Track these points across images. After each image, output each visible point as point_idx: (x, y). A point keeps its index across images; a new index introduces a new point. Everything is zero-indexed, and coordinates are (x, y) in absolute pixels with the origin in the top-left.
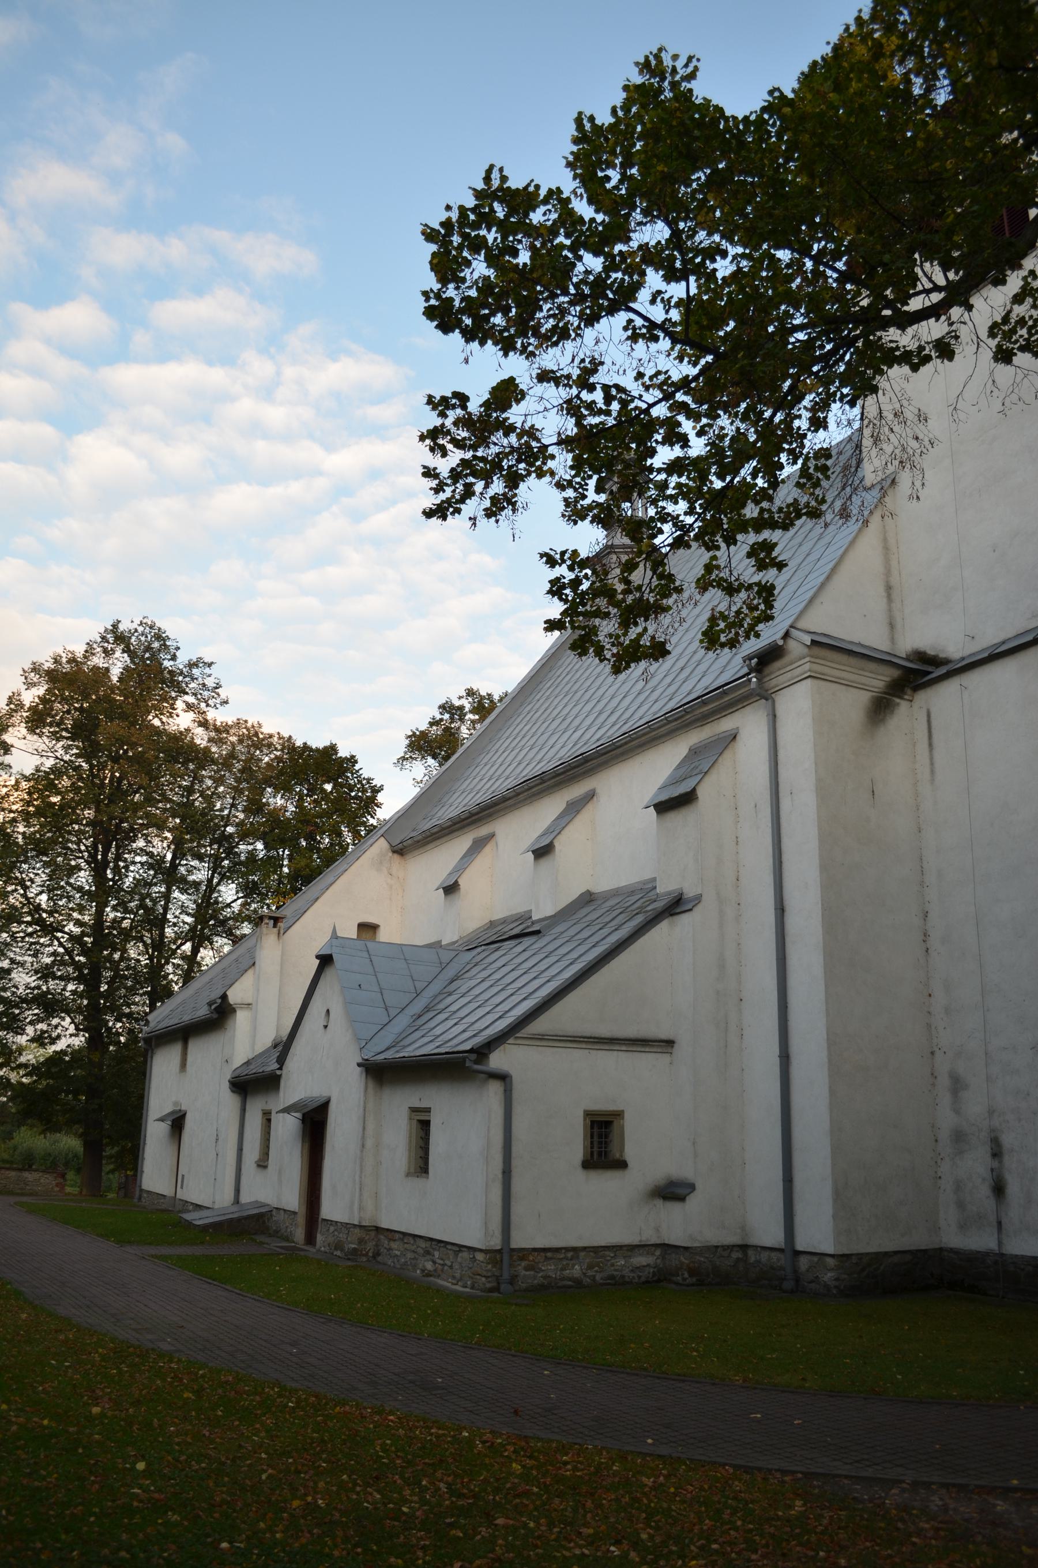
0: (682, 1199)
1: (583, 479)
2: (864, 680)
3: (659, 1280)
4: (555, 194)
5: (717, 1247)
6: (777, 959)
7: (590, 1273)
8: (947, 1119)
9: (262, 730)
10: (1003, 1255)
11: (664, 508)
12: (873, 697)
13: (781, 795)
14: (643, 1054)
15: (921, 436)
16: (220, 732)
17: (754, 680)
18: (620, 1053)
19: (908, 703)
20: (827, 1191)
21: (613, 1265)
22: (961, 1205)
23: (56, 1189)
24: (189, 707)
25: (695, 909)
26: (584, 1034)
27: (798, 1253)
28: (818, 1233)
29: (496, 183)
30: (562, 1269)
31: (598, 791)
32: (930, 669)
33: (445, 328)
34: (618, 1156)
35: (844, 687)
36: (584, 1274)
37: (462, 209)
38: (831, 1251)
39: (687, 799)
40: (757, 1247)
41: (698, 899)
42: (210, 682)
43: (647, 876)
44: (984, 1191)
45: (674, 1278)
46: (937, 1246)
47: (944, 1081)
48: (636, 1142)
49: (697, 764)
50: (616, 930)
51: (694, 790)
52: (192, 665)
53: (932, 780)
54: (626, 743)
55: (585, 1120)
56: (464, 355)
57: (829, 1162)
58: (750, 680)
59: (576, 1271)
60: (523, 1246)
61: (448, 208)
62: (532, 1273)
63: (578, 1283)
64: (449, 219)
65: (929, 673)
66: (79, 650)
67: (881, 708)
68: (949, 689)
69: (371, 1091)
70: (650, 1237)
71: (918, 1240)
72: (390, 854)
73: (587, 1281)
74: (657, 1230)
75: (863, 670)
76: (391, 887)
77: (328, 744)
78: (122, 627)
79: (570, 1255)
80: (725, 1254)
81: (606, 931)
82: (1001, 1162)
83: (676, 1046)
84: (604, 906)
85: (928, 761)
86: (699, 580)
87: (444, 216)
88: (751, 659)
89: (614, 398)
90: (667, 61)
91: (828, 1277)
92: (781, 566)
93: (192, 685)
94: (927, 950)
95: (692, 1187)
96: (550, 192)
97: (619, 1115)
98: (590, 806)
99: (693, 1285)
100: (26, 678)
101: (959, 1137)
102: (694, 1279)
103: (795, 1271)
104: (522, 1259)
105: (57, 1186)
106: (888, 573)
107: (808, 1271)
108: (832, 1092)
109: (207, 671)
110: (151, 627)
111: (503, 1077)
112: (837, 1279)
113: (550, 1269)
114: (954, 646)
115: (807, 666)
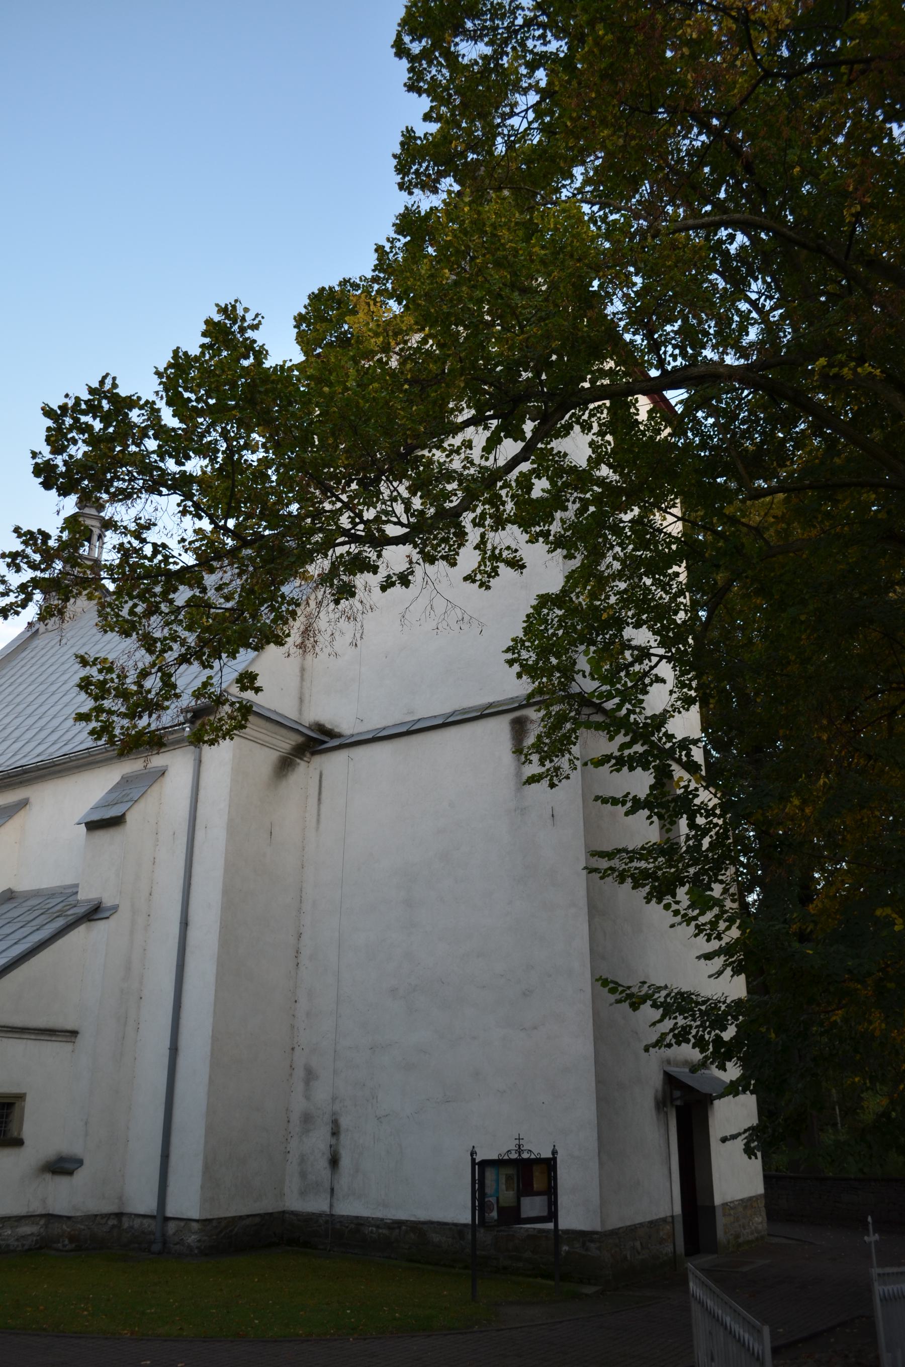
0: (70, 1173)
1: (121, 603)
2: (275, 741)
3: (41, 1247)
4: (150, 404)
5: (96, 1216)
6: (177, 965)
8: (298, 1104)
10: (332, 1215)
11: (176, 631)
12: (280, 756)
13: (197, 828)
14: (49, 1043)
15: (365, 601)
17: (188, 729)
18: (29, 1041)
20: (197, 1167)
22: (303, 1175)
25: (111, 918)
27: (167, 1219)
28: (187, 1202)
29: (108, 386)
31: (31, 800)
32: (326, 739)
33: (47, 485)
34: (15, 1134)
35: (259, 746)
37: (78, 399)
38: (196, 1216)
39: (117, 822)
40: (131, 1214)
41: (115, 909)
43: (69, 881)
44: (322, 1164)
45: (55, 1245)
46: (280, 1210)
47: (300, 1073)
49: (129, 792)
50: (38, 929)
51: (124, 815)
53: (317, 829)
54: (64, 763)
56: (57, 508)
58: (184, 729)
61: (67, 396)
64: (66, 404)
65: (325, 742)
67: (285, 765)
68: (340, 757)
70: (36, 1208)
71: (267, 1205)
80: (104, 1221)
81: (26, 930)
82: (338, 1140)
83: (79, 1036)
84: (24, 904)
86: (195, 691)
87: (62, 401)
88: (187, 712)
89: (160, 552)
90: (240, 312)
91: (191, 1239)
92: (258, 690)
95: (80, 1162)
96: (147, 402)
97: (21, 1097)
98: (22, 813)
99: (71, 1251)
101: (307, 1119)
103: (164, 1235)
107: (174, 1234)
108: (211, 1081)
112: (199, 1241)
114: (347, 726)
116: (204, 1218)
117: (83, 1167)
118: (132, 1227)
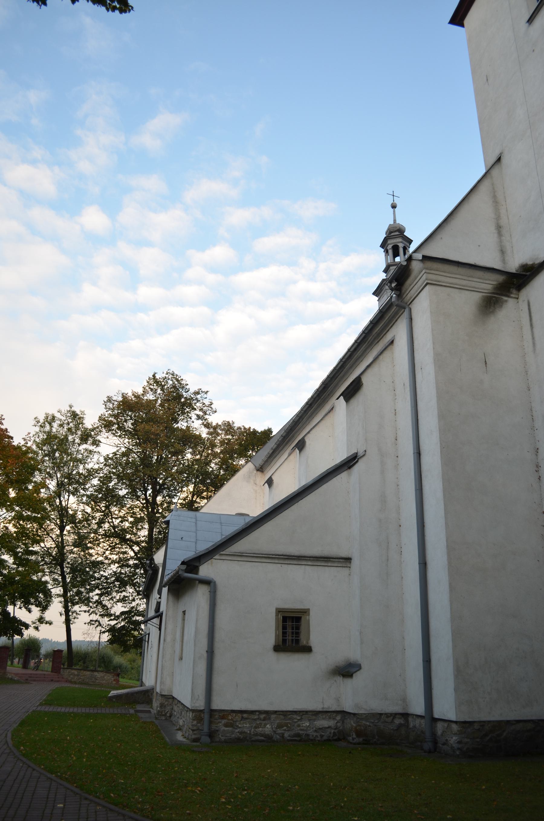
2: (473, 284)
3: (339, 737)
5: (381, 714)
7: (279, 731)
9: (234, 425)
12: (483, 296)
13: (416, 372)
14: (326, 568)
16: (214, 430)
18: (307, 567)
19: (515, 300)
21: (299, 726)
23: (114, 682)
24: (199, 418)
26: (278, 553)
30: (256, 727)
36: (275, 732)
38: (453, 718)
40: (414, 715)
42: (207, 402)
48: (317, 633)
52: (197, 393)
55: (277, 615)
57: (451, 644)
59: (268, 729)
60: (223, 708)
62: (230, 729)
63: (269, 739)
66: (140, 391)
67: (490, 304)
69: (171, 603)
70: (330, 705)
72: (255, 472)
73: (277, 737)
74: (338, 700)
75: (472, 277)
76: (256, 491)
77: (266, 428)
78: (157, 377)
79: (262, 716)
80: (390, 719)
83: (352, 561)
85: (530, 337)
93: (198, 404)
94: (539, 478)
97: (306, 612)
100: (106, 405)
102: (361, 739)
103: (434, 734)
104: (223, 718)
105: (114, 680)
106: (498, 217)
109: (205, 396)
110: (173, 375)
111: (207, 582)
112: (459, 742)
113: (246, 727)
115: (424, 277)
116: (462, 720)
117: (362, 671)
118: (415, 726)
